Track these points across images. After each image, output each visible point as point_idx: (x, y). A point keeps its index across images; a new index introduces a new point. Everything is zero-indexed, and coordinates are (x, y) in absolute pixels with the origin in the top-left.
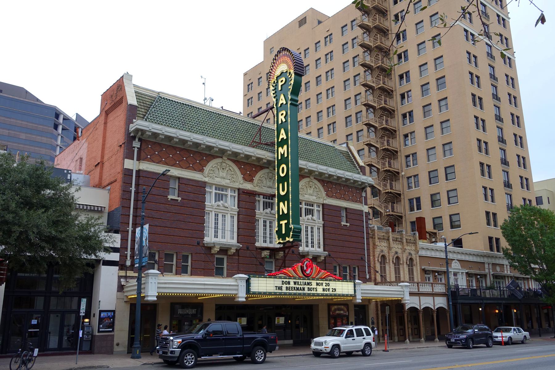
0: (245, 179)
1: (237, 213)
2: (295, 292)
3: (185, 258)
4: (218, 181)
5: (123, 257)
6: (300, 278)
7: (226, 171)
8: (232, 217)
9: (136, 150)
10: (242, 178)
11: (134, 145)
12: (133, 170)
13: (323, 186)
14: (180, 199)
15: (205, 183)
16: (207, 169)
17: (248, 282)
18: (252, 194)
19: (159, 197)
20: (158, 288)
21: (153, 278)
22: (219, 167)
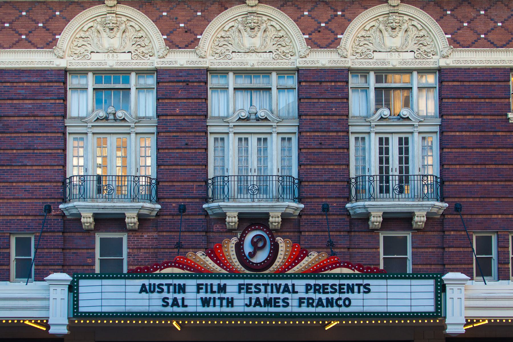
0: (172, 44)
6: (234, 274)
7: (119, 34)
8: (286, 140)
10: (163, 43)
13: (440, 19)
15: (65, 72)
16: (64, 39)
18: (339, 76)
20: (467, 308)
21: (455, 288)
22: (382, 27)
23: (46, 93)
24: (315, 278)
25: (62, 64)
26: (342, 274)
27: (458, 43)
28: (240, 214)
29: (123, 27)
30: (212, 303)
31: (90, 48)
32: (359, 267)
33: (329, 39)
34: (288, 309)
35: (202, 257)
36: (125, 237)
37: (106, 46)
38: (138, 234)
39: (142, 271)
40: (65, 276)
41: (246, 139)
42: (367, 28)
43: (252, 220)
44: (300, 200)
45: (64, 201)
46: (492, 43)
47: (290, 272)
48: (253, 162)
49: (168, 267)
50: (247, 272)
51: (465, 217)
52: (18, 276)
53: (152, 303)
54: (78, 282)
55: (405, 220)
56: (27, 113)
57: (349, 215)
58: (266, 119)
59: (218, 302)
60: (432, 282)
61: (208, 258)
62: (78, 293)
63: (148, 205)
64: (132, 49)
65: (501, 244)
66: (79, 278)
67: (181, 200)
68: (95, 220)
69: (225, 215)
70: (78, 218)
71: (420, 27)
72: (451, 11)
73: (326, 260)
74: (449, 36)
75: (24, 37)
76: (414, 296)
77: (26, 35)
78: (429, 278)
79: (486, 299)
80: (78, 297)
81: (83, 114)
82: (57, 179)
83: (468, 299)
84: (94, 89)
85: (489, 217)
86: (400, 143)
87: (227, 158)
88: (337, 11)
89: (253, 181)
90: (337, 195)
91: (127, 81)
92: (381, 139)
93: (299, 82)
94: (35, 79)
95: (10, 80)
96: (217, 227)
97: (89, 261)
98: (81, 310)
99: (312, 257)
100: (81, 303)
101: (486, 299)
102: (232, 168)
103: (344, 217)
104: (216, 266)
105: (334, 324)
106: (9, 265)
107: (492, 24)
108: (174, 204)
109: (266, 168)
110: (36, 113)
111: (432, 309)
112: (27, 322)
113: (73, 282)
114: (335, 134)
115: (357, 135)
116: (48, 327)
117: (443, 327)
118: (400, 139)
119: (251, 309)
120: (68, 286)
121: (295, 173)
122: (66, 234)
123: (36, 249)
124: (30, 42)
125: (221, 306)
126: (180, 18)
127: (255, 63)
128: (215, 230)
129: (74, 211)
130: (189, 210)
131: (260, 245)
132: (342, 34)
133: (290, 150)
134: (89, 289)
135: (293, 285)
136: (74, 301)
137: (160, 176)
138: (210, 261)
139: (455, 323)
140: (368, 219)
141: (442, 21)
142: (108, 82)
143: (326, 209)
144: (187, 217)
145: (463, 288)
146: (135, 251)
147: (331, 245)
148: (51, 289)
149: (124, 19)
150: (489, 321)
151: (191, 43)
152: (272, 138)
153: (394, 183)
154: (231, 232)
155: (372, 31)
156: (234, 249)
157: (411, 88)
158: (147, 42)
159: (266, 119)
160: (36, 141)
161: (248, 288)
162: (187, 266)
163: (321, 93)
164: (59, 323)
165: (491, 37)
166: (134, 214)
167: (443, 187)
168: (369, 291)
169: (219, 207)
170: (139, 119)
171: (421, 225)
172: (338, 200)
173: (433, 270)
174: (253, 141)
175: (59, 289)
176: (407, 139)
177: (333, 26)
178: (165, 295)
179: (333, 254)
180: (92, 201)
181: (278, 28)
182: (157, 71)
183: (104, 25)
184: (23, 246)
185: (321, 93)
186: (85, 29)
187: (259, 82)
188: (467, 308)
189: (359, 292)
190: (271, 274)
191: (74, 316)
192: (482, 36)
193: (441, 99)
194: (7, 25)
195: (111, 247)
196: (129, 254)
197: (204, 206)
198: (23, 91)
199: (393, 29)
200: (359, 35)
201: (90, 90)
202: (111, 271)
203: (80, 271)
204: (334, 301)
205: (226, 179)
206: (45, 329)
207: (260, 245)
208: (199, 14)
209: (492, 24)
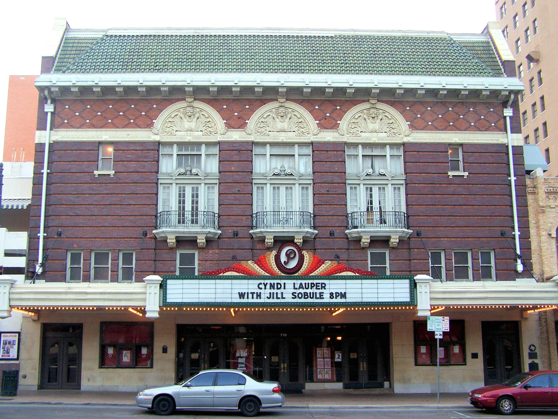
0: (229, 126)
1: (403, 182)
2: (303, 300)
3: (486, 257)
5: (32, 261)
6: (273, 276)
7: (287, 120)
9: (508, 119)
10: (224, 125)
11: (46, 110)
12: (507, 146)
13: (403, 112)
14: (466, 174)
15: (159, 143)
16: (158, 123)
17: (163, 286)
19: (82, 174)
21: (423, 285)
25: (157, 138)
28: (274, 237)
29: (197, 115)
32: (358, 271)
33: (332, 123)
35: (252, 265)
37: (279, 127)
39: (211, 274)
40: (157, 278)
43: (281, 241)
44: (315, 228)
45: (156, 228)
47: (311, 275)
48: (283, 204)
49: (229, 271)
50: (282, 274)
51: (423, 239)
55: (384, 241)
56: (132, 170)
57: (348, 238)
58: (292, 174)
59: (250, 296)
60: (407, 281)
62: (166, 289)
63: (212, 230)
65: (448, 257)
67: (235, 228)
68: (304, 241)
69: (265, 237)
70: (165, 241)
74: (409, 123)
75: (132, 121)
76: (396, 291)
77: (134, 120)
80: (166, 292)
81: (169, 171)
82: (152, 214)
84: (177, 155)
85: (439, 239)
86: (193, 190)
87: (265, 201)
89: (283, 215)
91: (199, 150)
93: (313, 151)
94: (138, 148)
96: (259, 246)
97: (172, 269)
98: (168, 301)
99: (327, 264)
100: (168, 296)
103: (344, 239)
105: (342, 310)
106: (118, 271)
108: (230, 231)
109: (292, 207)
111: (408, 300)
112: (130, 309)
113: (162, 281)
114: (337, 185)
116: (144, 312)
118: (193, 188)
119: (271, 300)
121: (311, 210)
122: (157, 251)
124: (136, 124)
126: (235, 110)
128: (258, 248)
129: (163, 235)
130: (239, 236)
131: (292, 256)
133: (307, 196)
134: (175, 286)
136: (163, 294)
140: (360, 241)
142: (187, 150)
143: (236, 234)
144: (239, 239)
147: (337, 257)
148: (148, 286)
149: (198, 110)
151: (242, 125)
152: (295, 188)
153: (188, 216)
154: (269, 249)
155: (359, 119)
156: (274, 259)
157: (386, 156)
158: (213, 125)
159: (292, 174)
160: (138, 188)
163: (328, 158)
164: (153, 311)
165: (435, 124)
166: (203, 237)
167: (409, 219)
168: (293, 294)
169: (261, 232)
170: (207, 175)
172: (340, 228)
173: (406, 272)
175: (153, 286)
177: (334, 115)
180: (175, 228)
181: (299, 116)
183: (185, 114)
184: (127, 259)
185: (328, 158)
186: (173, 116)
187: (287, 151)
192: (430, 123)
193: (405, 162)
194: (121, 113)
196: (199, 264)
198: (130, 156)
201: (175, 156)
202: (187, 274)
203: (168, 275)
205: (265, 213)
206: (141, 315)
207: (292, 256)
209: (435, 116)
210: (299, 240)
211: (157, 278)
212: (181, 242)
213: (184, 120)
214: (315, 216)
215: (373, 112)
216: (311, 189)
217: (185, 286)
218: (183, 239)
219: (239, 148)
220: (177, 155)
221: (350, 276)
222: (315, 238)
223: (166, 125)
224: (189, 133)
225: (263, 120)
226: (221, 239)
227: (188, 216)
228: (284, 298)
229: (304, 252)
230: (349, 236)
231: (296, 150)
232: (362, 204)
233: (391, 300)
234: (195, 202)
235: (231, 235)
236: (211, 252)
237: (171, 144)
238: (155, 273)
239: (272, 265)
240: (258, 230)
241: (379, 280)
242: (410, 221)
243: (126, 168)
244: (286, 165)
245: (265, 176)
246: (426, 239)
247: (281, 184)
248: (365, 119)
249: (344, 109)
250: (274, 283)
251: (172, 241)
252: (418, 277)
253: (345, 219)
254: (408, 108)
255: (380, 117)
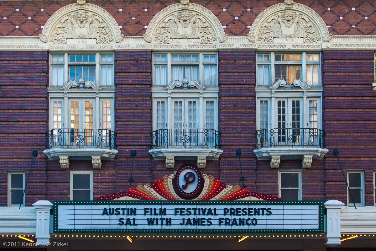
0: (126, 33)
4: (174, 45)
6: (171, 201)
7: (87, 25)
10: (119, 32)
13: (322, 14)
15: (48, 52)
16: (47, 29)
20: (342, 226)
23: (34, 69)
24: (231, 204)
25: (45, 47)
26: (251, 201)
27: (336, 32)
28: (176, 157)
29: (297, 19)
30: (155, 223)
31: (66, 36)
33: (241, 28)
34: (211, 227)
35: (148, 189)
36: (91, 174)
37: (78, 33)
38: (101, 172)
39: (104, 199)
40: (48, 203)
41: (181, 102)
42: (269, 21)
43: (185, 162)
44: (220, 147)
46: (361, 32)
47: (212, 199)
48: (186, 119)
50: (181, 199)
51: (341, 159)
52: (14, 202)
53: (112, 222)
54: (57, 207)
57: (256, 158)
60: (316, 207)
61: (152, 189)
62: (57, 215)
64: (97, 36)
65: (368, 179)
66: (58, 204)
68: (70, 161)
70: (57, 160)
71: (307, 19)
72: (331, 8)
73: (239, 191)
74: (329, 27)
75: (17, 27)
77: (19, 26)
78: (314, 204)
79: (356, 219)
80: (57, 218)
81: (61, 84)
82: (42, 131)
83: (343, 219)
86: (293, 105)
87: (167, 116)
88: (247, 8)
90: (247, 143)
91: (93, 59)
92: (279, 102)
93: (219, 61)
94: (25, 58)
95: (8, 59)
96: (159, 167)
97: (65, 191)
98: (59, 227)
99: (229, 189)
100: (59, 223)
101: (356, 219)
102: (170, 123)
104: (159, 195)
105: (245, 238)
106: (6, 194)
107: (361, 18)
108: (128, 149)
110: (26, 83)
111: (316, 227)
112: (20, 237)
113: (53, 207)
115: (279, 100)
117: (325, 240)
118: (293, 102)
120: (50, 210)
121: (216, 127)
122: (48, 172)
123: (26, 182)
125: (162, 224)
127: (187, 46)
129: (54, 155)
131: (191, 179)
132: (251, 25)
133: (212, 110)
135: (215, 209)
137: (117, 129)
138: (154, 192)
139: (334, 237)
140: (270, 161)
141: (324, 15)
142: (79, 60)
144: (137, 159)
145: (339, 212)
146: (99, 184)
148: (38, 212)
150: (359, 235)
152: (199, 102)
154: (170, 170)
155: (272, 23)
156: (171, 183)
157: (301, 65)
160: (26, 104)
161: (181, 212)
162: (137, 195)
165: (359, 27)
166: (99, 157)
167: (325, 136)
170: (102, 88)
171: (309, 165)
174: (185, 103)
175: (43, 212)
176: (298, 102)
177: (244, 19)
178: (121, 216)
179: (244, 187)
182: (116, 53)
183: (76, 18)
184: (17, 181)
185: (236, 69)
186: (62, 21)
188: (342, 226)
189: (263, 214)
190: (216, 201)
191: (54, 232)
192: (354, 26)
193: (323, 72)
194: (5, 18)
195: (81, 181)
196: (95, 187)
197: (150, 151)
198: (17, 67)
199: (82, 22)
200: (263, 26)
201: (66, 66)
202: (81, 199)
203: (59, 199)
204: (245, 221)
205: (166, 131)
207: (191, 179)
208: (146, 10)
209: (361, 18)
210: (202, 161)
211: (48, 203)
212: (287, 162)
213: (76, 25)
214: (220, 133)
215: (185, 14)
216: (216, 102)
217: (303, 212)
218: (76, 159)
219: (137, 58)
220: (275, 65)
221: (254, 201)
222: (220, 158)
223: (55, 32)
224: (81, 40)
225: (60, 25)
226: (118, 160)
227: (289, 134)
228: (137, 225)
229: (205, 176)
230: (258, 156)
231: (305, 59)
232: (273, 120)
233: (298, 227)
234: (296, 117)
235: (129, 155)
236: (107, 173)
237: (61, 53)
238: (46, 197)
239: (170, 189)
240: (158, 150)
241: (285, 206)
242: (326, 138)
243: (12, 81)
244: (191, 77)
245: (164, 88)
246: (344, 159)
247: (81, 98)
248: (72, 23)
249: (255, 11)
250: (205, 209)
251: (97, 162)
252: (329, 202)
253: (253, 138)
254: (329, 9)
255: (297, 19)
